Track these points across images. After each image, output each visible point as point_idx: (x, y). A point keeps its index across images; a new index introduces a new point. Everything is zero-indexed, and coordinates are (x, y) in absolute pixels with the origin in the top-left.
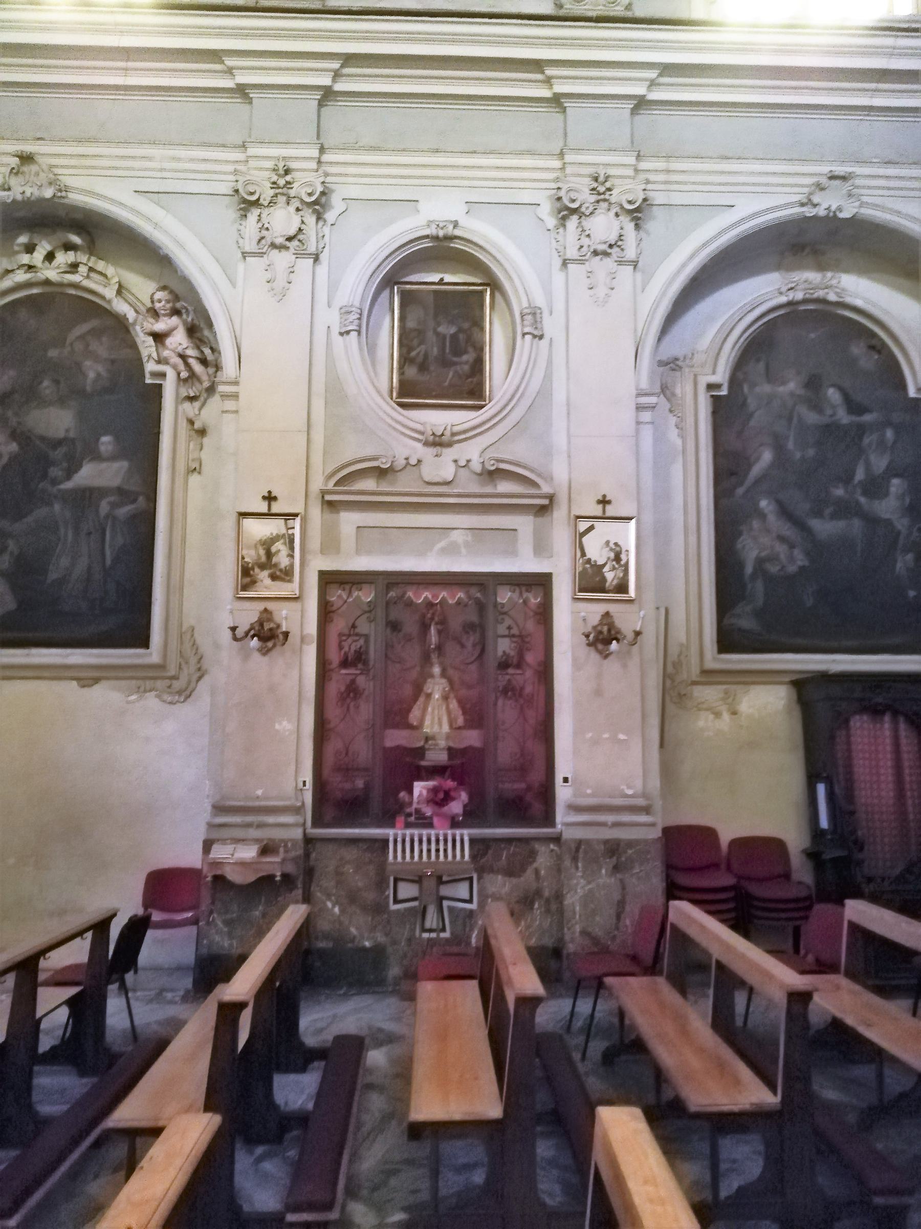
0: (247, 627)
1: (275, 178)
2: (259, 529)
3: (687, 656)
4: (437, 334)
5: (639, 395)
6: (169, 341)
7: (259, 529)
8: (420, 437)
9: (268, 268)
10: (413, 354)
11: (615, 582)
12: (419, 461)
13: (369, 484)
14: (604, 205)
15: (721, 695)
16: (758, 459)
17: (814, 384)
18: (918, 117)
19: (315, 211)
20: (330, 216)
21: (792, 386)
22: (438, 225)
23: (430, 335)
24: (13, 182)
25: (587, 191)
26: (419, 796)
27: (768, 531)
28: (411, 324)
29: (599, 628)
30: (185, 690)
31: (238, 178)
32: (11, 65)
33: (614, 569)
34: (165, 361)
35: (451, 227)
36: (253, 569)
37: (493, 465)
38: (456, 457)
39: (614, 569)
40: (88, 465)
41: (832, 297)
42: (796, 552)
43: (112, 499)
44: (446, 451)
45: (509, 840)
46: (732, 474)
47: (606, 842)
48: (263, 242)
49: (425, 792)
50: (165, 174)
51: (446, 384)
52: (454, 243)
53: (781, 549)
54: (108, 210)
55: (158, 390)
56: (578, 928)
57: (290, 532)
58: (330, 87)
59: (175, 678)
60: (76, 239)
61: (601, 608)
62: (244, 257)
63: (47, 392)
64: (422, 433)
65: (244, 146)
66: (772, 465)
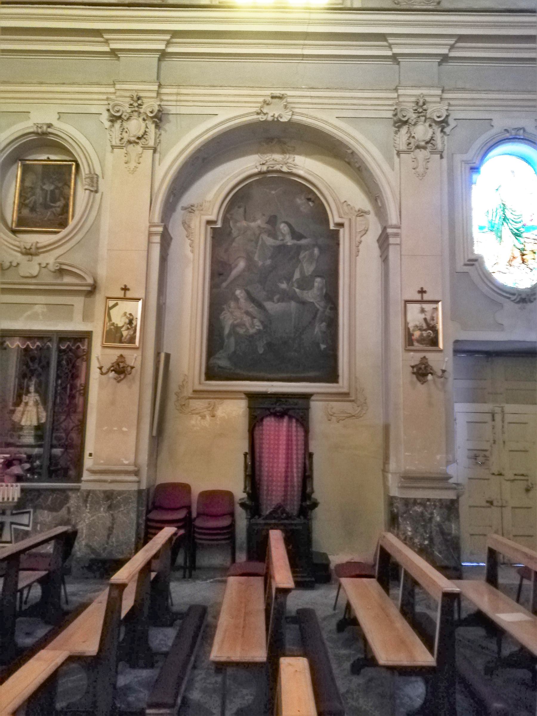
3: (187, 382)
4: (43, 189)
5: (150, 226)
8: (19, 249)
10: (27, 201)
11: (128, 336)
12: (18, 264)
14: (136, 114)
15: (207, 405)
16: (236, 265)
17: (272, 221)
18: (535, 64)
19: (154, 122)
20: (447, 130)
21: (259, 222)
23: (38, 191)
25: (128, 105)
27: (239, 308)
29: (420, 366)
31: (110, 102)
33: (128, 329)
35: (45, 127)
37: (57, 266)
38: (39, 262)
39: (128, 329)
41: (285, 169)
42: (256, 321)
44: (35, 258)
45: (53, 490)
46: (220, 274)
47: (105, 492)
48: (123, 140)
52: (50, 137)
53: (247, 319)
56: (84, 543)
58: (164, 50)
61: (118, 352)
62: (113, 148)
64: (18, 247)
65: (396, 90)
66: (244, 270)
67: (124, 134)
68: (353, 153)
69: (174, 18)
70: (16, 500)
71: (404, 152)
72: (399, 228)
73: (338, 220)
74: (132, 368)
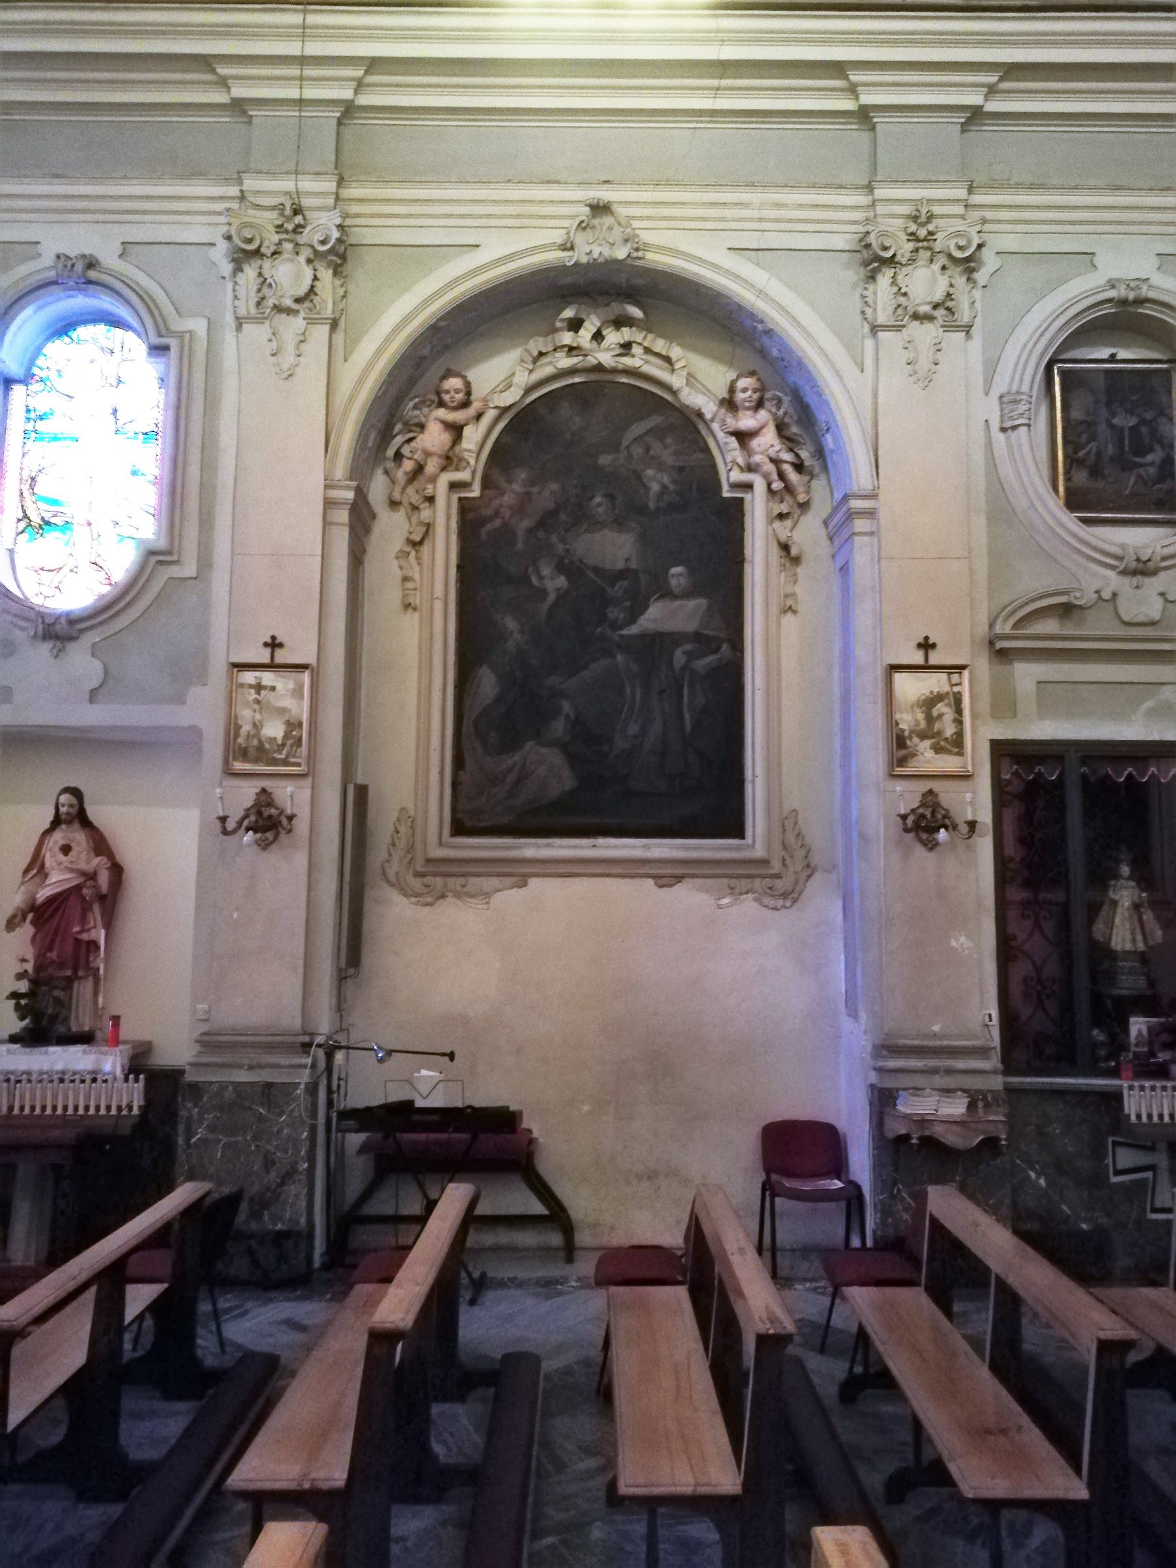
0: (240, 814)
1: (913, 227)
2: (910, 687)
4: (1112, 426)
6: (755, 443)
7: (910, 687)
9: (907, 345)
10: (1081, 453)
12: (1115, 595)
13: (1050, 626)
18: (1172, 127)
19: (330, 264)
20: (981, 277)
22: (1128, 285)
23: (1102, 428)
24: (580, 239)
25: (273, 230)
26: (1137, 1037)
28: (1076, 414)
29: (921, 811)
30: (792, 892)
32: (446, 86)
34: (750, 468)
36: (910, 738)
40: (656, 604)
43: (688, 647)
44: (1148, 581)
49: (1145, 1032)
50: (766, 226)
51: (1127, 492)
54: (696, 274)
55: (737, 506)
57: (956, 689)
58: (353, 101)
59: (778, 876)
60: (635, 312)
63: (600, 510)
67: (265, 290)
68: (769, 332)
69: (249, 26)
70: (136, 1111)
71: (249, 319)
72: (873, 496)
73: (736, 476)
74: (291, 818)
